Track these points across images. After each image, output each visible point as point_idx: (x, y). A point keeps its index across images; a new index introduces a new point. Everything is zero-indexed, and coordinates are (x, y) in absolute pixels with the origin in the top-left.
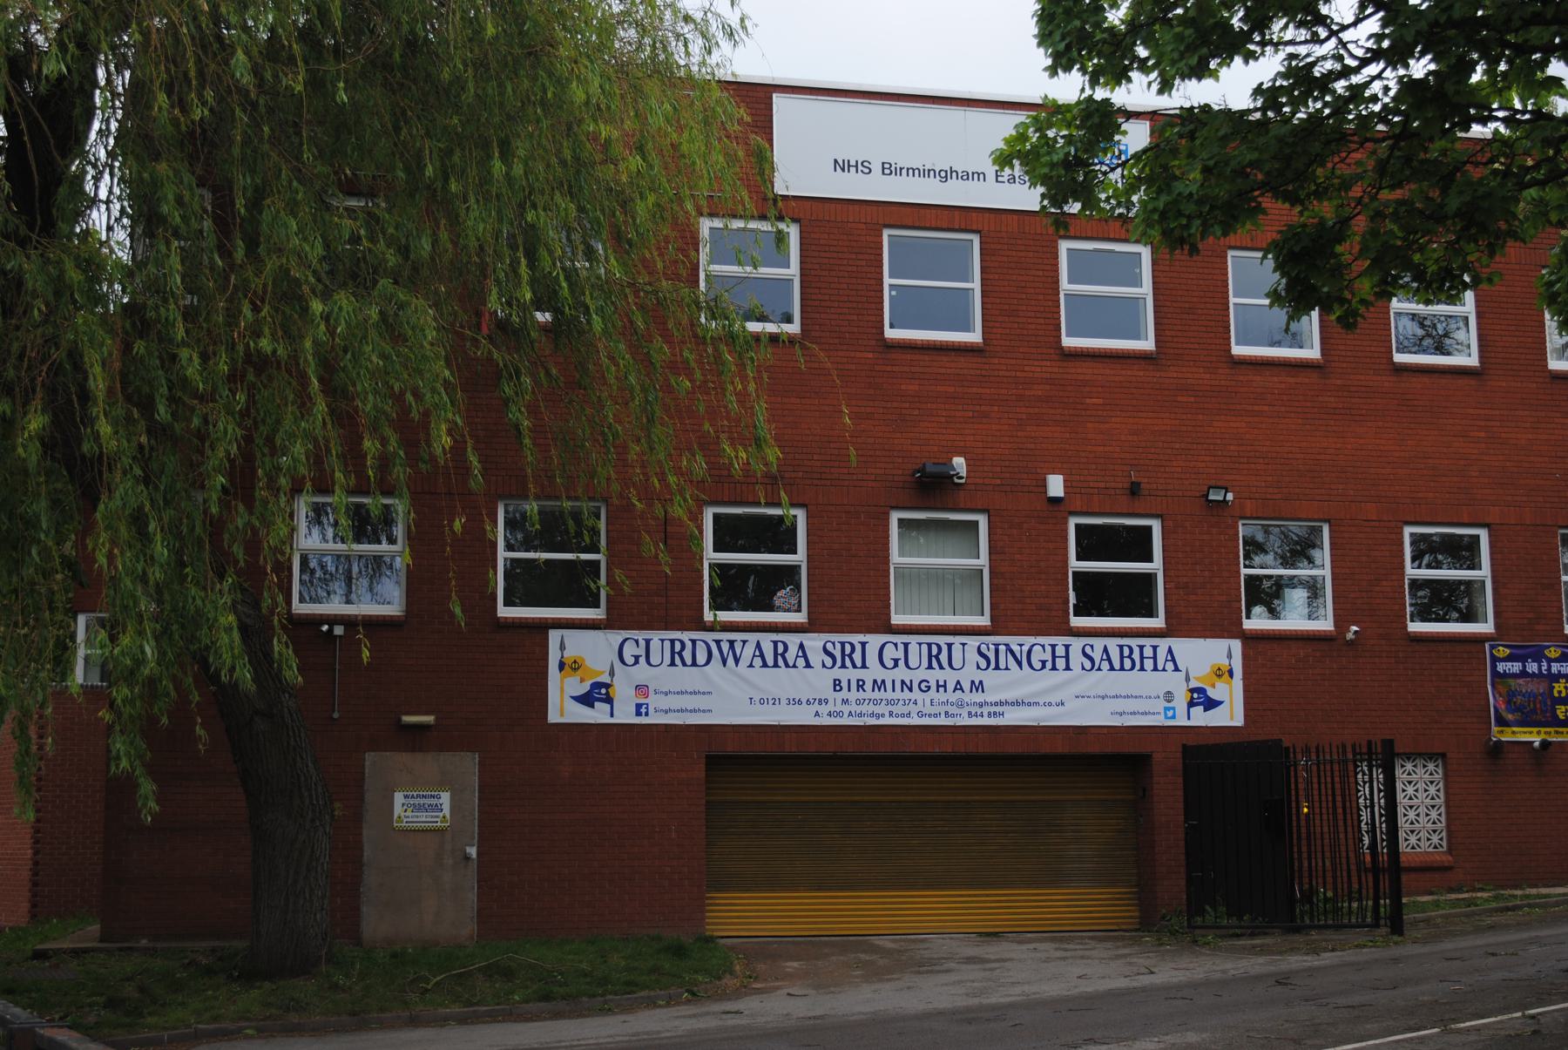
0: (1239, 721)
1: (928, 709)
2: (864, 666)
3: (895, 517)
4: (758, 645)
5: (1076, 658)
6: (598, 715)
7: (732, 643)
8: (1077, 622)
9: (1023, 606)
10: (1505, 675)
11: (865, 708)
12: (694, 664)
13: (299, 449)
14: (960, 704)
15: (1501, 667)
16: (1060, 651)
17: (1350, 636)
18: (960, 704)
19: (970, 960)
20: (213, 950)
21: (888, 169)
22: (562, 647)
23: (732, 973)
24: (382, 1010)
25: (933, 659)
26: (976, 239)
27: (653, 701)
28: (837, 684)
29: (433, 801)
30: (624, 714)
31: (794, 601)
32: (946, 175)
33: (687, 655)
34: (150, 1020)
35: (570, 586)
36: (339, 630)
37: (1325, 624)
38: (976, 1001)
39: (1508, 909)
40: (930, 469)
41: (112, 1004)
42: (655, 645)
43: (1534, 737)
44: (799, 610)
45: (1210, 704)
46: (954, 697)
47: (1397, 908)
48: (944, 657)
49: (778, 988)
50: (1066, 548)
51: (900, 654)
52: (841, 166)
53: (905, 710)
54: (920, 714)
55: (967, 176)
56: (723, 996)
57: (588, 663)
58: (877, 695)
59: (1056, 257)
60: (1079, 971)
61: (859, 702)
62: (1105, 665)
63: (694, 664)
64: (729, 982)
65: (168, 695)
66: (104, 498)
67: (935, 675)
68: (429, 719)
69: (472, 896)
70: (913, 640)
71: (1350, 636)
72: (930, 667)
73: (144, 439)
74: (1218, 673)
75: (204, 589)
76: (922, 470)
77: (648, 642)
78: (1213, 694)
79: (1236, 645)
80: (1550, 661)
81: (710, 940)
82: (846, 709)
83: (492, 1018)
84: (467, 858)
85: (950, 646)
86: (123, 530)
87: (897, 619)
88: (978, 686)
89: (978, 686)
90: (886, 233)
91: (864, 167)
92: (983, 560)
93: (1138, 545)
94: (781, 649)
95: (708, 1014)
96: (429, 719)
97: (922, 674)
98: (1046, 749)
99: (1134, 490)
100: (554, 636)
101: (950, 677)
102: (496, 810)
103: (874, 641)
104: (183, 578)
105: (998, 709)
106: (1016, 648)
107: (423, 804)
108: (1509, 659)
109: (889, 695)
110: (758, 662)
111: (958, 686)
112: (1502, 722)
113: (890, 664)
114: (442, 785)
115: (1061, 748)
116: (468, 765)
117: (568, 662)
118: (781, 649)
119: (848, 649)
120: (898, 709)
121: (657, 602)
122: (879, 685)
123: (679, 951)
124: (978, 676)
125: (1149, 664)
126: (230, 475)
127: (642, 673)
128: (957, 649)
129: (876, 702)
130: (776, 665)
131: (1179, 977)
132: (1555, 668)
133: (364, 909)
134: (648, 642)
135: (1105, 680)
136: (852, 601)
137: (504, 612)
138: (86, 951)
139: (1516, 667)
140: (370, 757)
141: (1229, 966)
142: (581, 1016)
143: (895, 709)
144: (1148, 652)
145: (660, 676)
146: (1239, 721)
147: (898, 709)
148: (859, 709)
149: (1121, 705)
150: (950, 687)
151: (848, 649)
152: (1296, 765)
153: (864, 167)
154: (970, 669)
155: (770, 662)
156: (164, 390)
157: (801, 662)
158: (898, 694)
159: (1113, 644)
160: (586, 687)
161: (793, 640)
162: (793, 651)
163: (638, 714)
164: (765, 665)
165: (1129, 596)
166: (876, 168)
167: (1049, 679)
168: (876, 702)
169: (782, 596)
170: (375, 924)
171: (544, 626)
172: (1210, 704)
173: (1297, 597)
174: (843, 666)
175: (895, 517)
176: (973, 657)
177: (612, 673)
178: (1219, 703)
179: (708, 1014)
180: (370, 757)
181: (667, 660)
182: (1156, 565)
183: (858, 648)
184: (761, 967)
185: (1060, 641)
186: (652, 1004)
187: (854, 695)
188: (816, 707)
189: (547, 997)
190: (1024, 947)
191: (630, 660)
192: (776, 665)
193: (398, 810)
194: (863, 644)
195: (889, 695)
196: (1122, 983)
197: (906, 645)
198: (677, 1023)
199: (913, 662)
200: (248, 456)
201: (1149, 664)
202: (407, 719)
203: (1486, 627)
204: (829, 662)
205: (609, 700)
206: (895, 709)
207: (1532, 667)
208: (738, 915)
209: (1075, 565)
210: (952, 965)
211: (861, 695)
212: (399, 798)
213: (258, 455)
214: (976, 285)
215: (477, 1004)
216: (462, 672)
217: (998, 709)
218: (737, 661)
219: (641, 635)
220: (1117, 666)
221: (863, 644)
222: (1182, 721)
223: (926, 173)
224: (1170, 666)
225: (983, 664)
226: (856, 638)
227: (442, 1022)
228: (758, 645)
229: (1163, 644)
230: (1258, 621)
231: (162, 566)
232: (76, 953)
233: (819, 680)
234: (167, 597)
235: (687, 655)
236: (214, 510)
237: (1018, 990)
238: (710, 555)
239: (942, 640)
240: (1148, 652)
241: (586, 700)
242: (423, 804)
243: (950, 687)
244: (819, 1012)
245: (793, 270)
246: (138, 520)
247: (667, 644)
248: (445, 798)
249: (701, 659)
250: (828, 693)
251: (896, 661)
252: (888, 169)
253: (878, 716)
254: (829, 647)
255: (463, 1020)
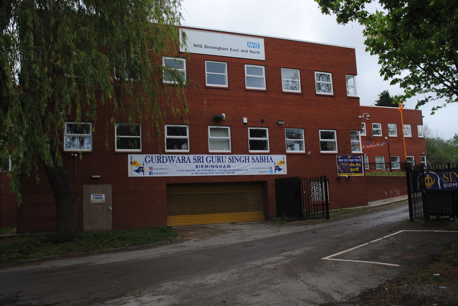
0: (286, 173)
1: (218, 172)
2: (203, 162)
3: (209, 127)
4: (178, 157)
5: (251, 160)
6: (140, 175)
7: (172, 157)
8: (251, 151)
9: (239, 147)
10: (340, 162)
11: (203, 172)
12: (163, 162)
13: (68, 96)
14: (225, 171)
15: (339, 160)
16: (247, 158)
17: (309, 154)
18: (225, 171)
19: (233, 230)
20: (46, 235)
21: (206, 47)
22: (131, 159)
23: (178, 236)
24: (93, 250)
25: (219, 160)
26: (226, 64)
27: (154, 171)
28: (197, 166)
29: (101, 196)
30: (147, 174)
31: (186, 147)
32: (219, 49)
33: (161, 160)
34: (31, 256)
35: (134, 144)
36: (76, 155)
37: (303, 151)
38: (243, 241)
39: (345, 213)
40: (217, 116)
41: (20, 252)
42: (154, 158)
43: (346, 175)
44: (187, 149)
45: (280, 169)
46: (223, 169)
47: (328, 212)
48: (221, 160)
49: (190, 239)
50: (248, 134)
51: (211, 159)
52: (195, 46)
53: (213, 172)
54: (216, 173)
55: (224, 49)
56: (178, 242)
57: (138, 162)
58: (206, 169)
59: (244, 68)
60: (264, 231)
61: (202, 170)
62: (257, 161)
63: (163, 162)
64: (179, 238)
65: (29, 168)
66: (10, 109)
67: (219, 164)
68: (99, 176)
69: (111, 219)
70: (214, 156)
71: (309, 154)
72: (218, 162)
73: (22, 92)
74: (281, 162)
75: (40, 137)
76: (216, 116)
77: (152, 157)
78: (280, 167)
79: (285, 156)
80: (349, 159)
81: (170, 227)
82: (199, 172)
83: (122, 251)
84: (109, 210)
85: (222, 157)
86: (15, 119)
87: (210, 151)
88: (229, 166)
89: (229, 166)
90: (206, 62)
91: (200, 46)
92: (229, 137)
93: (262, 134)
94: (183, 158)
95: (177, 247)
96: (99, 176)
97: (216, 164)
98: (244, 180)
99: (262, 121)
100: (129, 156)
101: (222, 164)
102: (116, 198)
103: (205, 156)
104: (34, 134)
105: (233, 171)
106: (237, 157)
107: (98, 197)
108: (340, 159)
109: (209, 169)
110: (178, 161)
111: (224, 166)
112: (340, 172)
113: (209, 161)
114: (102, 192)
115: (248, 180)
116: (109, 187)
117: (133, 162)
118: (183, 158)
119: (199, 158)
120: (211, 172)
121: (153, 148)
122: (206, 166)
123: (164, 231)
124: (229, 164)
125: (266, 161)
126: (49, 103)
127: (151, 164)
128: (224, 158)
129: (206, 170)
130: (182, 162)
131: (288, 232)
132: (350, 160)
133: (84, 223)
134: (152, 157)
135: (257, 164)
136: (200, 147)
137: (117, 150)
138: (13, 236)
139: (342, 160)
140: (84, 186)
141: (296, 229)
142: (144, 249)
143: (210, 172)
144: (266, 158)
145: (155, 165)
146: (286, 173)
147: (211, 172)
148: (202, 172)
149: (260, 170)
150: (223, 166)
151: (199, 158)
152: (302, 182)
153: (200, 46)
154: (227, 162)
155: (181, 161)
156: (28, 78)
157: (188, 161)
158: (211, 168)
159: (258, 156)
160: (137, 168)
161: (186, 156)
162: (186, 159)
163: (150, 174)
164: (180, 162)
165: (261, 145)
166: (203, 46)
167: (245, 164)
168: (206, 170)
169: (184, 146)
170: (87, 227)
171: (127, 154)
172: (280, 169)
173: (297, 146)
174: (198, 162)
175: (209, 127)
176: (228, 160)
177: (144, 165)
178: (281, 169)
179: (177, 247)
180: (84, 186)
181: (157, 161)
182: (267, 138)
183: (201, 158)
184: (184, 234)
185: (247, 156)
186: (161, 245)
187: (201, 169)
188: (192, 172)
189: (135, 245)
190: (244, 226)
191: (148, 162)
192: (182, 162)
193: (92, 199)
194: (203, 157)
195: (209, 169)
196: (275, 234)
197: (212, 157)
198: (171, 250)
199: (214, 161)
200: (53, 97)
201: (266, 161)
202: (93, 176)
203: (336, 152)
204: (195, 161)
205: (143, 171)
206: (210, 172)
207: (345, 160)
208: (175, 221)
209: (250, 138)
210: (229, 231)
211: (202, 169)
212: (92, 196)
213: (56, 99)
214: (226, 74)
215: (118, 247)
216: (107, 165)
217: (233, 171)
218: (173, 161)
219: (150, 155)
220: (259, 161)
221: (203, 157)
222: (274, 173)
223: (215, 48)
224: (271, 161)
225: (230, 161)
226: (201, 156)
227: (109, 252)
228: (178, 157)
229: (269, 156)
230: (289, 151)
231: (26, 130)
232: (10, 237)
233: (192, 165)
234: (29, 139)
235: (161, 160)
236: (43, 114)
237: (251, 237)
238: (166, 136)
239: (221, 156)
240: (266, 158)
241: (138, 171)
242: (98, 197)
243: (223, 166)
244: (205, 245)
245: (185, 69)
246: (20, 116)
247: (157, 158)
248: (103, 196)
249: (165, 161)
250: (195, 168)
251: (210, 161)
252: (206, 47)
253: (206, 174)
254: (195, 158)
255: (114, 252)
